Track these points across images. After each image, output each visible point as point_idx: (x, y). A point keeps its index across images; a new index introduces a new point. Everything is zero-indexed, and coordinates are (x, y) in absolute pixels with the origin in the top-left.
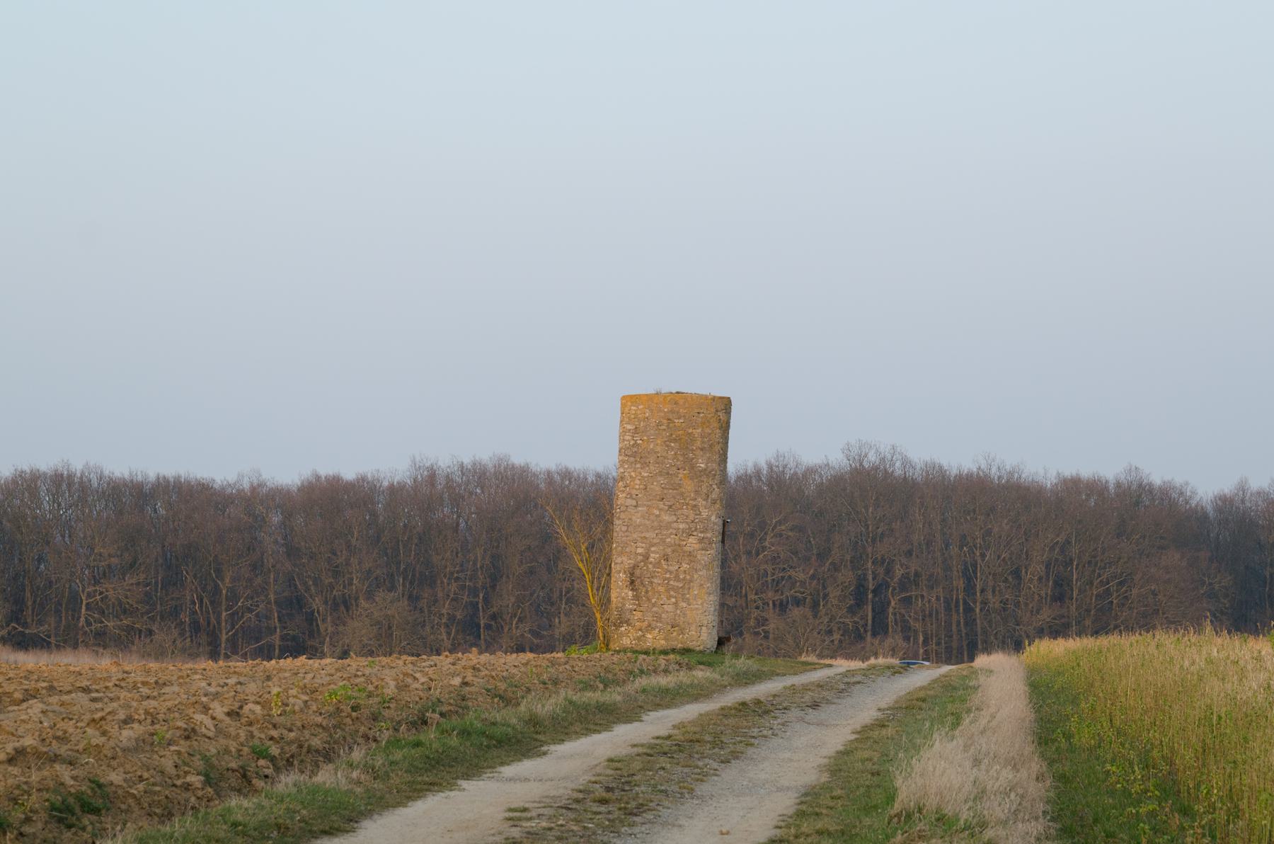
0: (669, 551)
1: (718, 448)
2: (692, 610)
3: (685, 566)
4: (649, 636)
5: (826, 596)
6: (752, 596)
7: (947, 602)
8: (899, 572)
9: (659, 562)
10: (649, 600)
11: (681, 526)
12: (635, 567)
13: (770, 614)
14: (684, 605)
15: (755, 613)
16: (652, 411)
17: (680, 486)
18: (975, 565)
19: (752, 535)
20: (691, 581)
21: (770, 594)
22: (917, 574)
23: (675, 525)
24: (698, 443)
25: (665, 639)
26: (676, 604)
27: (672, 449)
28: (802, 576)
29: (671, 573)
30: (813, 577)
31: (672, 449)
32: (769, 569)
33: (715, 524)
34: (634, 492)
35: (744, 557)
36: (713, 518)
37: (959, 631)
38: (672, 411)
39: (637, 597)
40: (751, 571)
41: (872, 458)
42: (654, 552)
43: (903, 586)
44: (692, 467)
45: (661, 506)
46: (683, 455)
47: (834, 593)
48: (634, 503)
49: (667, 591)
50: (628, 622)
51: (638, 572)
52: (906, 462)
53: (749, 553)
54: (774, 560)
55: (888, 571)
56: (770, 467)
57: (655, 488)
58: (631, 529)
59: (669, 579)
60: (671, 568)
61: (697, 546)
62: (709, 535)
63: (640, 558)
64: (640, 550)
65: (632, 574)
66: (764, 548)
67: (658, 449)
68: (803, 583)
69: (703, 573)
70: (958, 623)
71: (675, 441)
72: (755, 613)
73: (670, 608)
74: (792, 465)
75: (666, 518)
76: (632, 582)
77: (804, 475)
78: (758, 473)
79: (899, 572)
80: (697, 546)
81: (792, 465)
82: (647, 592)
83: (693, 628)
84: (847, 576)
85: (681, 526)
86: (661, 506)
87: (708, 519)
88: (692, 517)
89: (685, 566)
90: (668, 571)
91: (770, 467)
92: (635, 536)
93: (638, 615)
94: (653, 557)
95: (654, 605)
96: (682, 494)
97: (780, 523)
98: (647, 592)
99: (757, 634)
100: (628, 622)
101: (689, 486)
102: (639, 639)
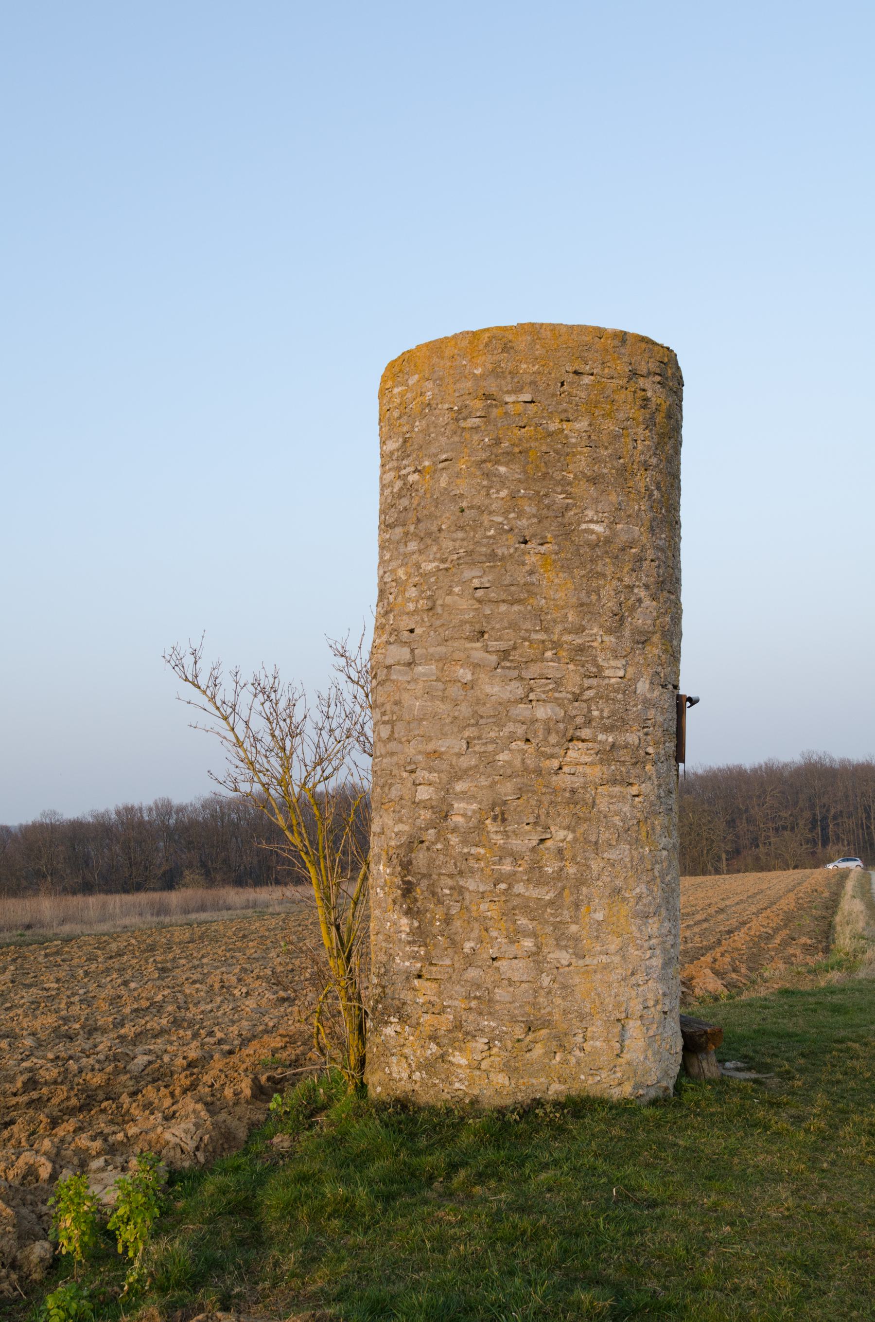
0: (507, 789)
1: (643, 481)
2: (588, 972)
3: (560, 835)
4: (459, 1059)
5: (798, 824)
6: (761, 826)
7: (857, 825)
8: (833, 812)
9: (480, 826)
10: (454, 944)
11: (542, 712)
12: (414, 842)
13: (771, 833)
14: (564, 957)
15: (764, 834)
16: (440, 381)
17: (530, 589)
18: (870, 807)
19: (759, 797)
20: (581, 881)
21: (770, 824)
22: (841, 812)
23: (522, 710)
24: (581, 463)
25: (509, 1069)
26: (536, 955)
27: (503, 481)
28: (785, 815)
29: (516, 858)
30: (791, 815)
31: (503, 481)
32: (769, 812)
33: (648, 703)
34: (406, 622)
35: (757, 807)
36: (643, 686)
37: (864, 838)
38: (496, 372)
39: (420, 935)
40: (760, 814)
41: (815, 757)
42: (464, 796)
43: (835, 818)
44: (567, 532)
45: (478, 655)
46: (538, 498)
47: (801, 823)
48: (404, 654)
49: (508, 914)
50: (401, 1013)
51: (420, 858)
52: (832, 760)
53: (759, 805)
54: (771, 807)
55: (828, 811)
56: (766, 764)
57: (460, 604)
58: (400, 730)
59: (511, 879)
60: (515, 843)
61: (596, 772)
62: (632, 738)
63: (426, 815)
64: (424, 793)
65: (406, 866)
66: (766, 802)
67: (462, 487)
68: (786, 818)
69: (622, 852)
70: (863, 834)
71: (510, 457)
72: (764, 834)
73: (516, 969)
74: (776, 763)
75: (496, 689)
76: (408, 890)
77: (783, 767)
78: (760, 767)
79: (833, 812)
80: (596, 772)
81: (776, 763)
82: (448, 920)
83: (597, 1027)
84: (807, 814)
85: (542, 712)
86: (478, 655)
87: (627, 688)
88: (573, 681)
89: (560, 835)
90: (505, 853)
91: (766, 764)
92: (410, 750)
93: (426, 990)
94: (463, 811)
95: (470, 960)
96: (539, 614)
97: (772, 790)
98: (448, 920)
99: (765, 844)
100: (401, 1013)
101: (558, 590)
102: (428, 1066)
